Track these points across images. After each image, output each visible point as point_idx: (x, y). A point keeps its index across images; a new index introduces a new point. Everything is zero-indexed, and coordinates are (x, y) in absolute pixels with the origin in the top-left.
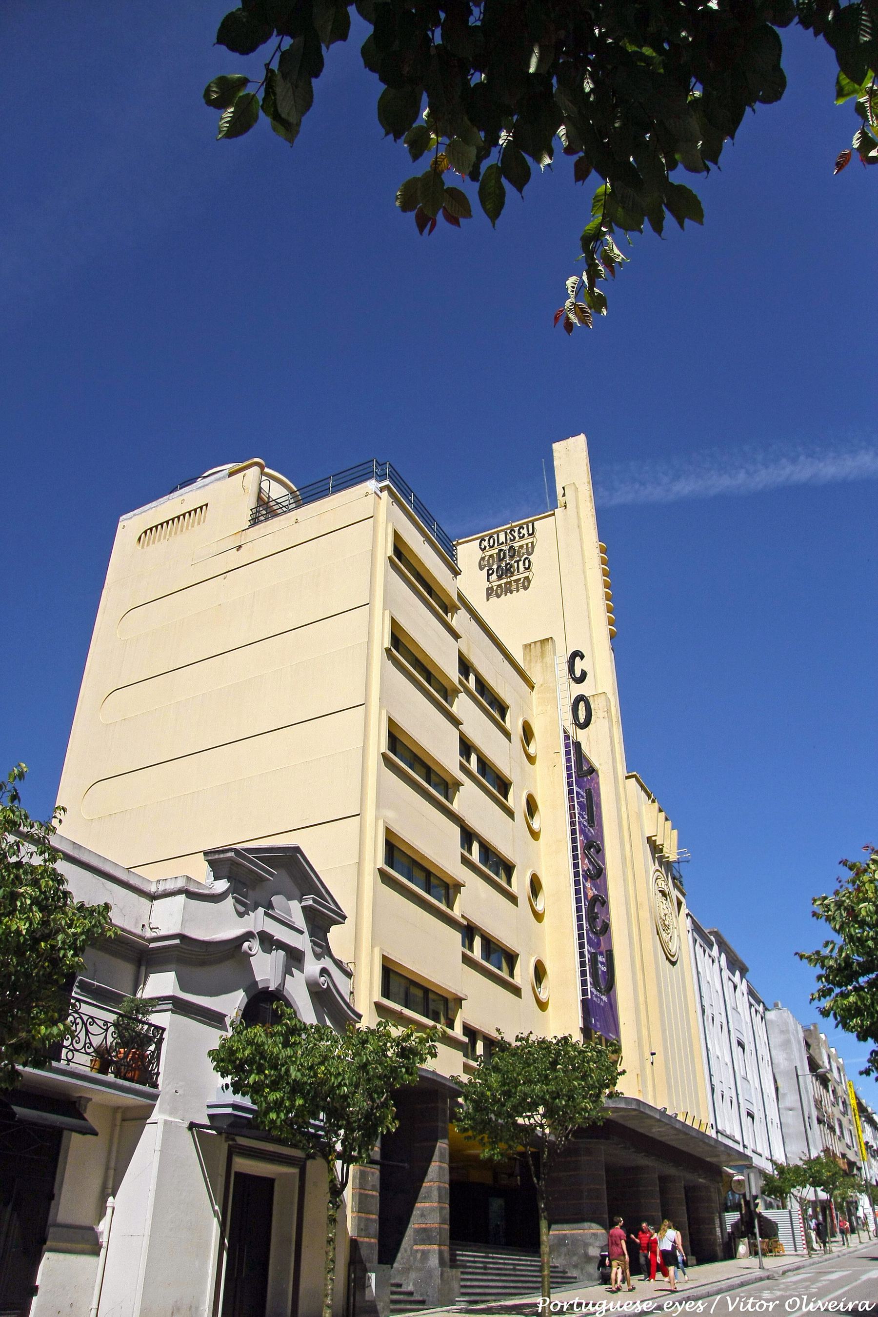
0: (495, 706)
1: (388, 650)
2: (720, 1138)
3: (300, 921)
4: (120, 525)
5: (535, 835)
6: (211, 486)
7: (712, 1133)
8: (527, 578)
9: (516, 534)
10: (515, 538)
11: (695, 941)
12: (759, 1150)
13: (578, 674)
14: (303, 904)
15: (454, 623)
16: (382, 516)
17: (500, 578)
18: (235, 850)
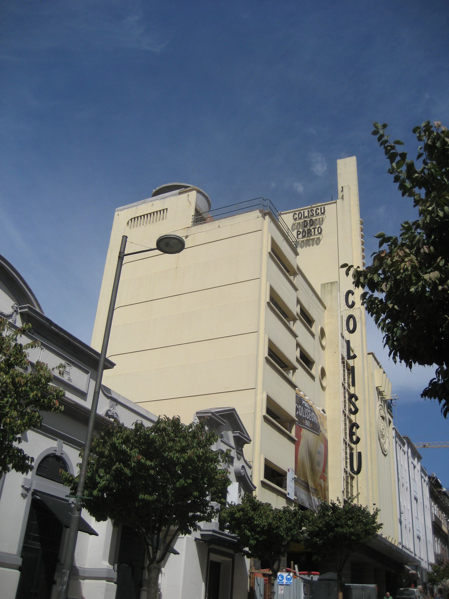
0: (308, 320)
1: (268, 303)
2: (404, 549)
3: (232, 442)
4: (116, 213)
5: (323, 388)
6: (168, 199)
7: (400, 547)
8: (318, 238)
9: (314, 212)
10: (313, 214)
11: (396, 442)
12: (422, 557)
13: (350, 303)
14: (235, 435)
15: (295, 282)
16: (266, 229)
17: (304, 237)
18: (212, 413)
